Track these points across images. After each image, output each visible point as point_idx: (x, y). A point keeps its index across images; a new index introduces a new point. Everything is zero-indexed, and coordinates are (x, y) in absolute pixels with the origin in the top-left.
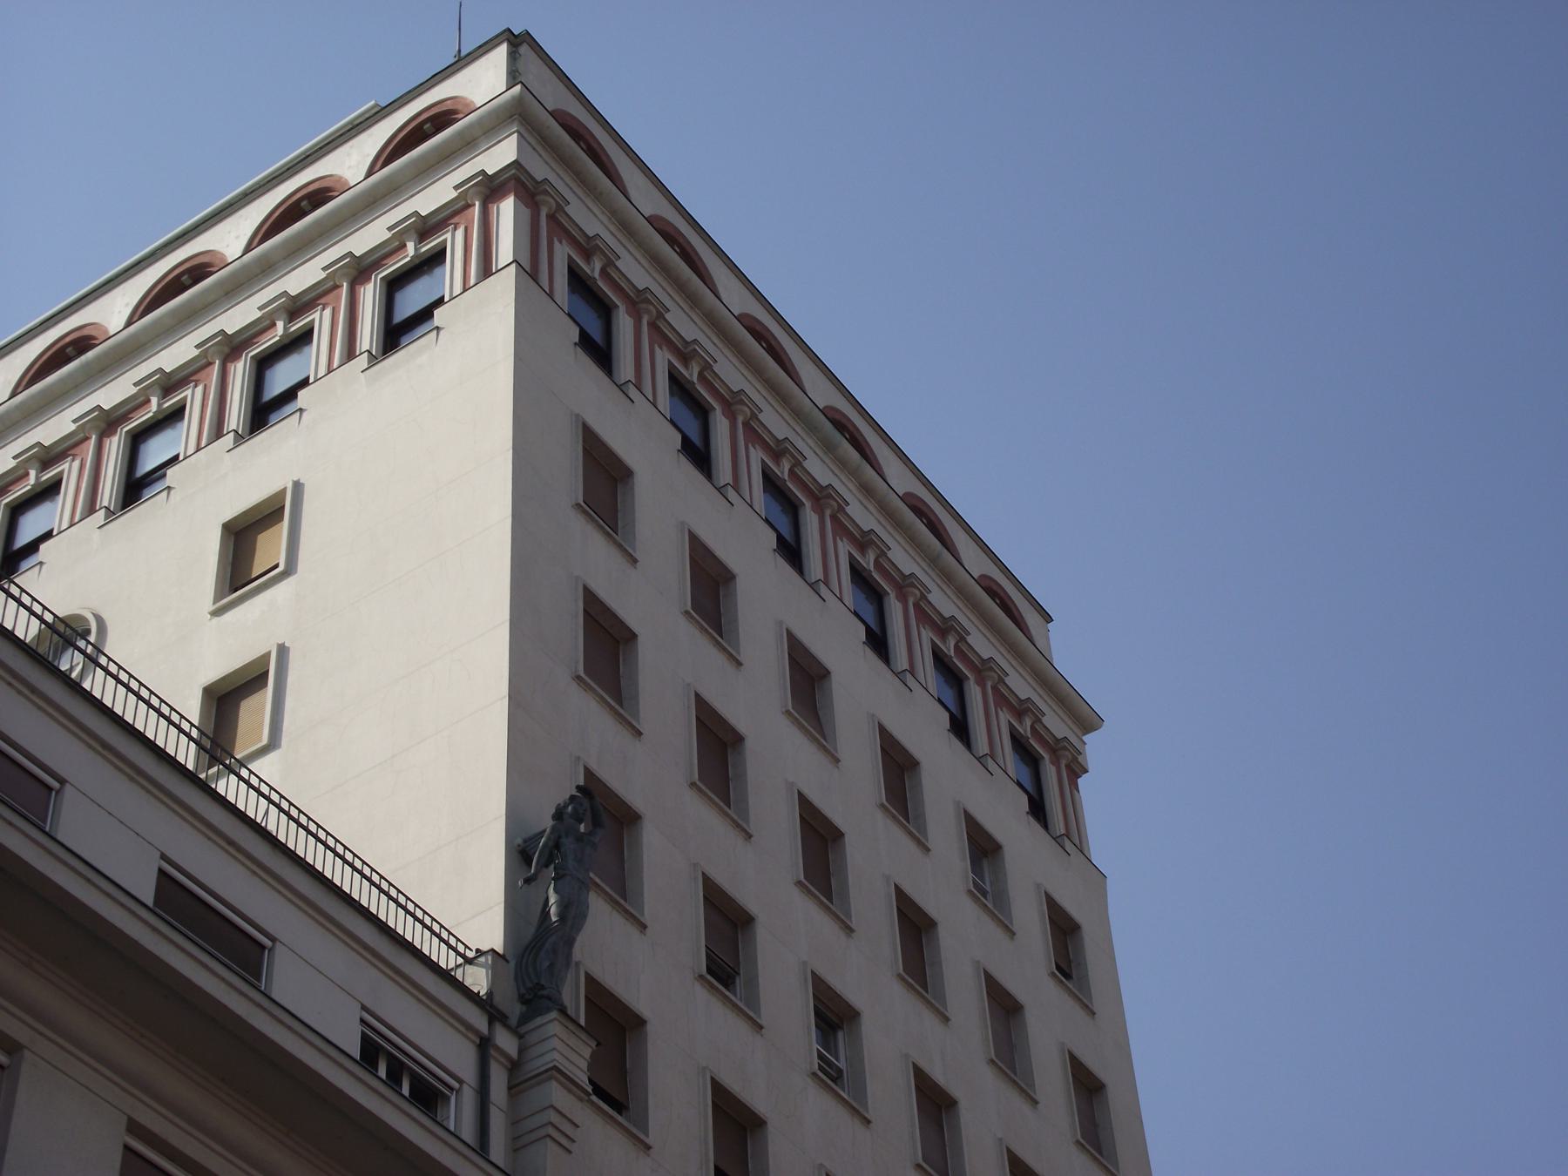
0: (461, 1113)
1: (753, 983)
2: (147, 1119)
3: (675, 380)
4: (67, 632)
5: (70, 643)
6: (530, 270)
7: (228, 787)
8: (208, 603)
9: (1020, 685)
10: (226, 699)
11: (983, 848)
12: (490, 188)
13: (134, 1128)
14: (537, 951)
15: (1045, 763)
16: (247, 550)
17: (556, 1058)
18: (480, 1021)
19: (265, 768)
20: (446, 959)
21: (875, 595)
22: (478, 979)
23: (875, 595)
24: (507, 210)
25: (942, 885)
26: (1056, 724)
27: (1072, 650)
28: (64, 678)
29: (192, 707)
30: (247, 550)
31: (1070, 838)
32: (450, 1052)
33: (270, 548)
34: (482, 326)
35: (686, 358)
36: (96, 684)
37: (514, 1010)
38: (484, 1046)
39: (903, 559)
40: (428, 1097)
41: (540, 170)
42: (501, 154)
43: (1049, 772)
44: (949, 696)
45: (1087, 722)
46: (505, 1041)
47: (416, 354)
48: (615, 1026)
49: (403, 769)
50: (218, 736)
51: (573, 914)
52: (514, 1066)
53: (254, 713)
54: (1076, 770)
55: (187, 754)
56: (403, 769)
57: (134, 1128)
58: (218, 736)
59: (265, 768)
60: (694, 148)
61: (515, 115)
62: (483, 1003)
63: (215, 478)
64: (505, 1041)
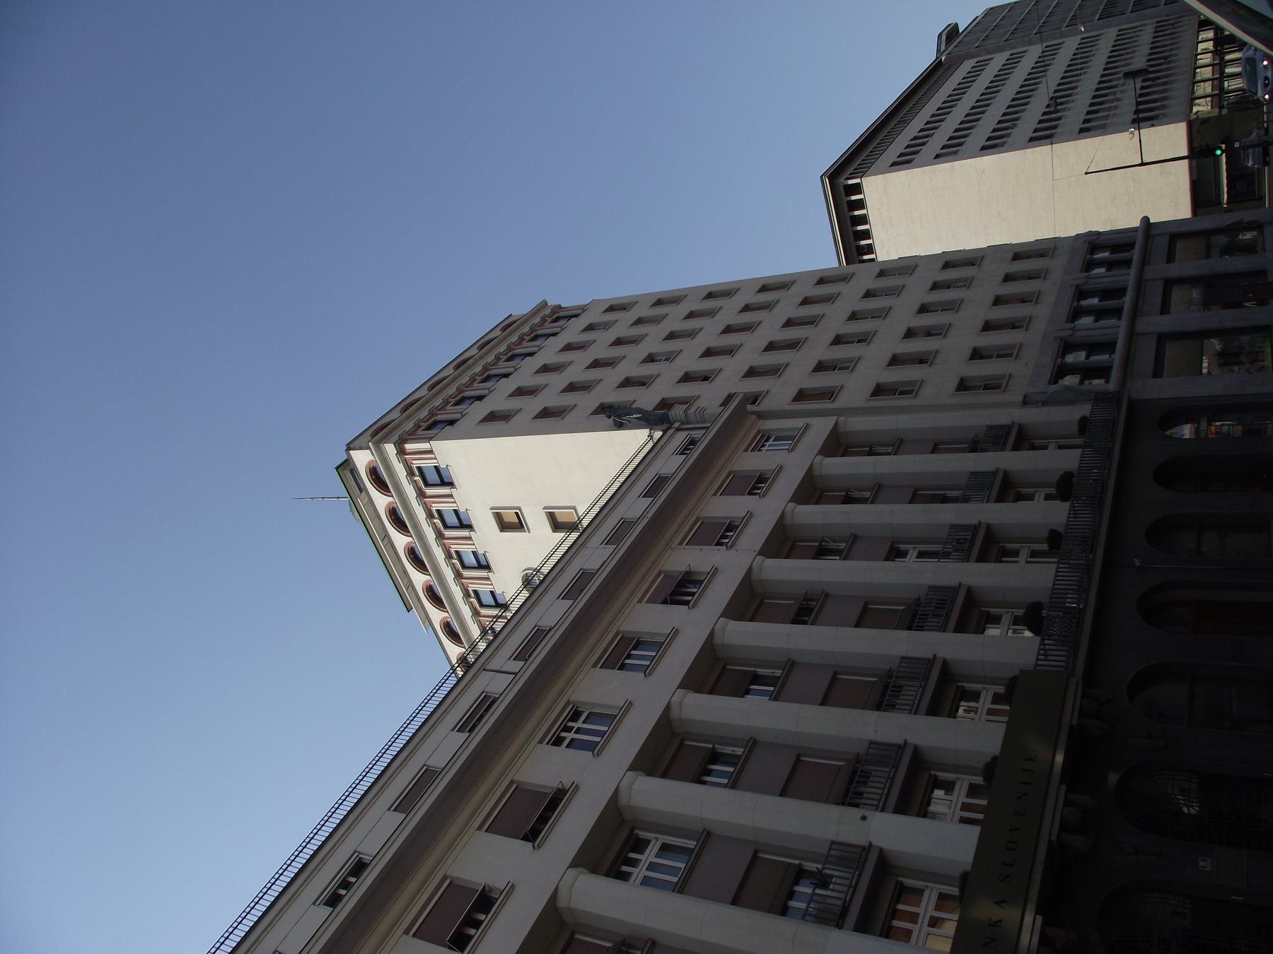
0: (697, 434)
1: (645, 377)
2: (713, 491)
3: (455, 404)
4: (527, 581)
5: (465, 658)
6: (430, 439)
7: (585, 523)
8: (526, 534)
9: (537, 320)
10: (557, 525)
11: (520, 392)
12: (401, 452)
13: (479, 828)
14: (648, 420)
15: (560, 316)
16: (511, 523)
17: (682, 412)
18: (671, 431)
19: (581, 511)
20: (650, 445)
21: (435, 423)
22: (658, 434)
23: (435, 423)
24: (409, 447)
25: (558, 381)
26: (547, 311)
27: (521, 308)
28: (541, 582)
29: (561, 535)
30: (511, 523)
31: (583, 309)
32: (681, 438)
33: (510, 517)
34: (450, 452)
35: (420, 427)
36: (545, 570)
37: (665, 426)
38: (678, 430)
39: (424, 414)
40: (693, 442)
41: (396, 438)
42: (390, 449)
43: (561, 314)
44: (441, 426)
45: (544, 304)
46: (676, 425)
47: (457, 475)
48: (665, 404)
49: (584, 466)
50: (570, 527)
51: (638, 411)
52: (683, 423)
53: (562, 516)
54: (560, 307)
55: (575, 535)
56: (584, 466)
57: (479, 828)
58: (570, 527)
59: (581, 511)
60: (382, 400)
61: (378, 445)
62: (665, 432)
63: (487, 537)
64: (676, 425)
